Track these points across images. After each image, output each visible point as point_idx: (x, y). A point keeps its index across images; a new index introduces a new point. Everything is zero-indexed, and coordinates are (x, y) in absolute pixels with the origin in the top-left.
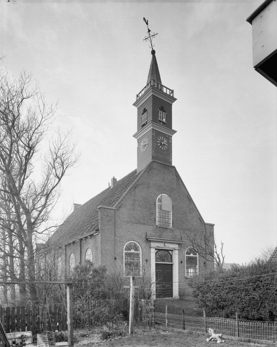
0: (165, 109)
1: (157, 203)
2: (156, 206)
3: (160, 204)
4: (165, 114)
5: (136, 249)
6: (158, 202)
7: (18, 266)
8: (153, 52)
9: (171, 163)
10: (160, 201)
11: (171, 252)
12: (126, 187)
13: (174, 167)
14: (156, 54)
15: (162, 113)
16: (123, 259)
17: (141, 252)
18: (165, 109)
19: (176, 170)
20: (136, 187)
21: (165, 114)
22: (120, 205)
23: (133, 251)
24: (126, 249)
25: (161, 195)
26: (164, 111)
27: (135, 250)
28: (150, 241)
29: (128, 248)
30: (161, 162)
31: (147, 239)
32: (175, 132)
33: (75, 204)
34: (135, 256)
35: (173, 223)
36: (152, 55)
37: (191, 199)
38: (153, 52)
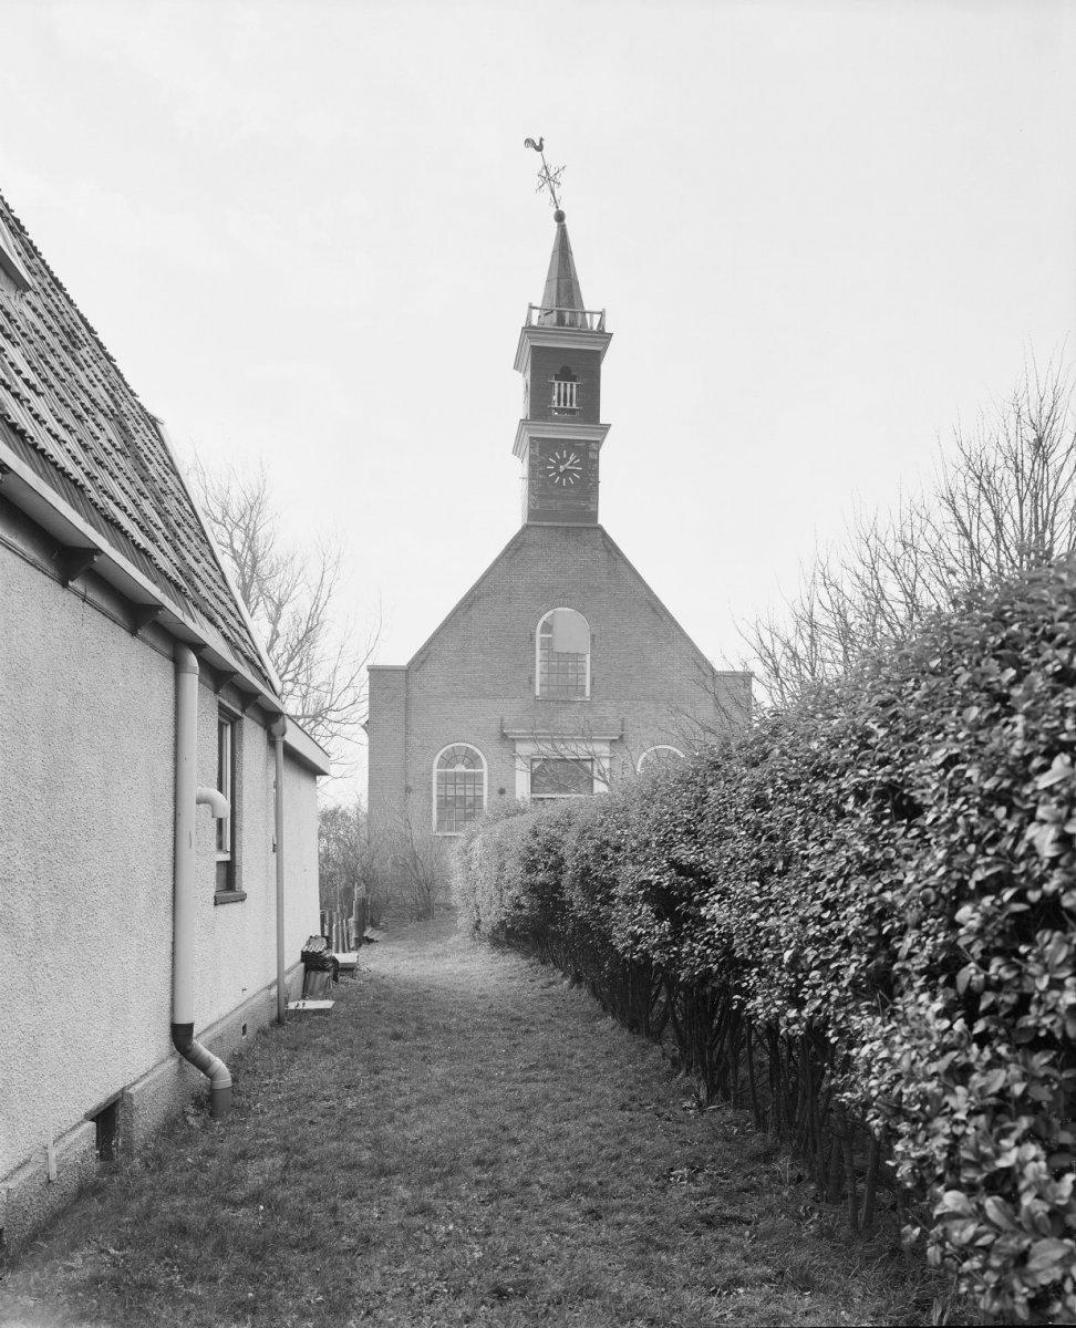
0: (573, 373)
1: (538, 636)
2: (534, 645)
3: (550, 636)
4: (575, 386)
5: (473, 760)
6: (542, 632)
7: (285, 1138)
8: (560, 217)
9: (594, 516)
10: (547, 628)
11: (589, 765)
12: (235, 647)
13: (600, 528)
14: (566, 221)
15: (569, 386)
16: (430, 789)
17: (485, 770)
18: (573, 373)
19: (605, 535)
20: (470, 606)
21: (575, 386)
22: (424, 656)
23: (460, 768)
24: (439, 766)
25: (551, 612)
26: (573, 379)
27: (467, 767)
28: (513, 740)
29: (448, 761)
30: (551, 524)
31: (504, 736)
32: (607, 427)
33: (373, 670)
34: (458, 781)
35: (592, 684)
36: (556, 224)
37: (663, 607)
38: (560, 217)
